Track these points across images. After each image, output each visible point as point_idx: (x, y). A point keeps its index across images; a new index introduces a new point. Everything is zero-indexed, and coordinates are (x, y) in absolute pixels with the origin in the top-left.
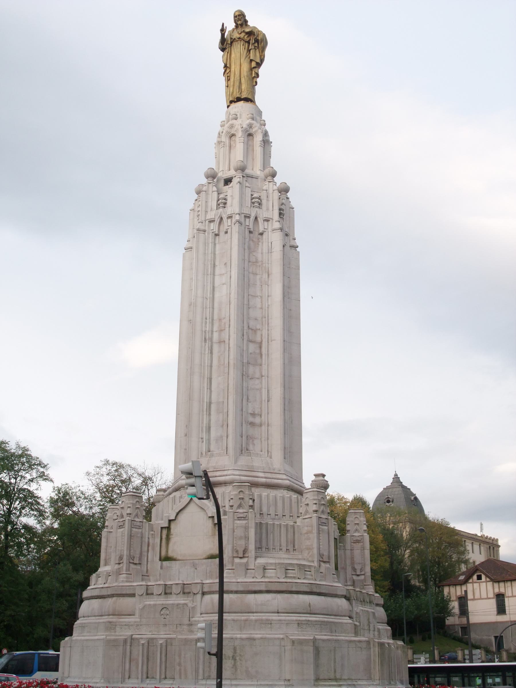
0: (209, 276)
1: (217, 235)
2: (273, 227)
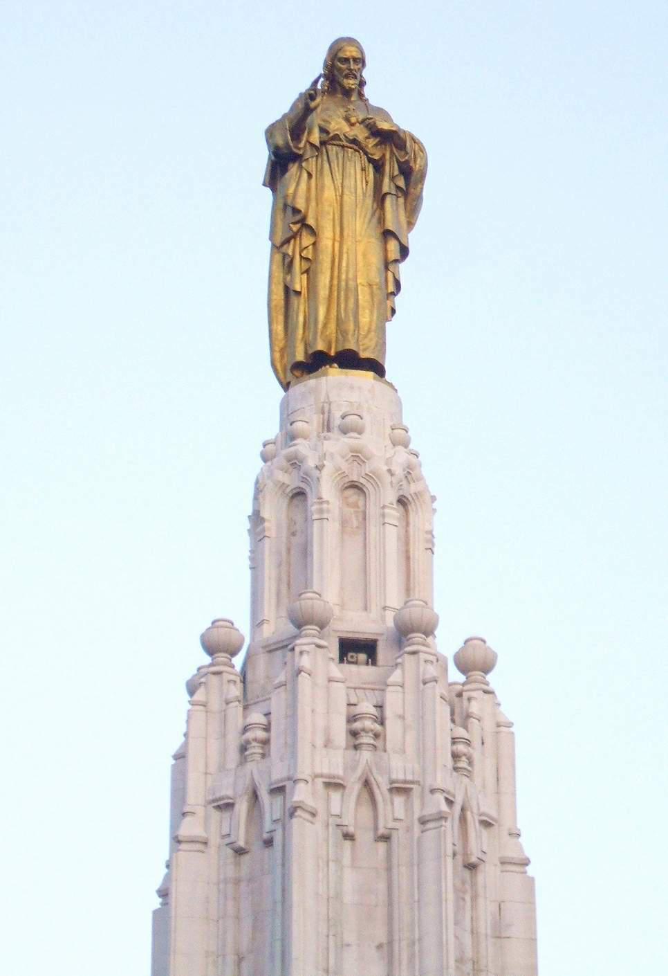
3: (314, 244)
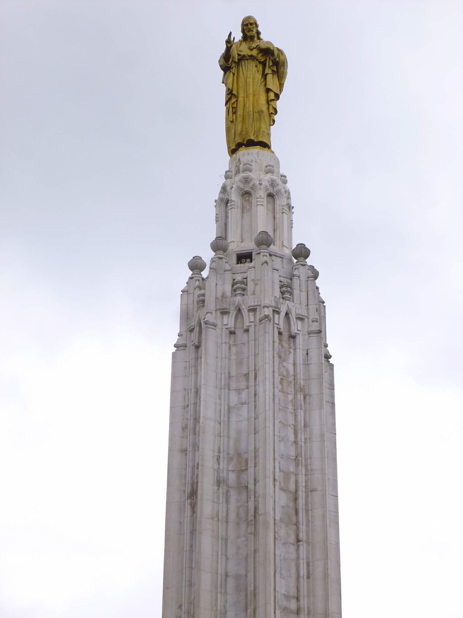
0: (223, 390)
1: (232, 333)
2: (310, 329)
3: (237, 101)
